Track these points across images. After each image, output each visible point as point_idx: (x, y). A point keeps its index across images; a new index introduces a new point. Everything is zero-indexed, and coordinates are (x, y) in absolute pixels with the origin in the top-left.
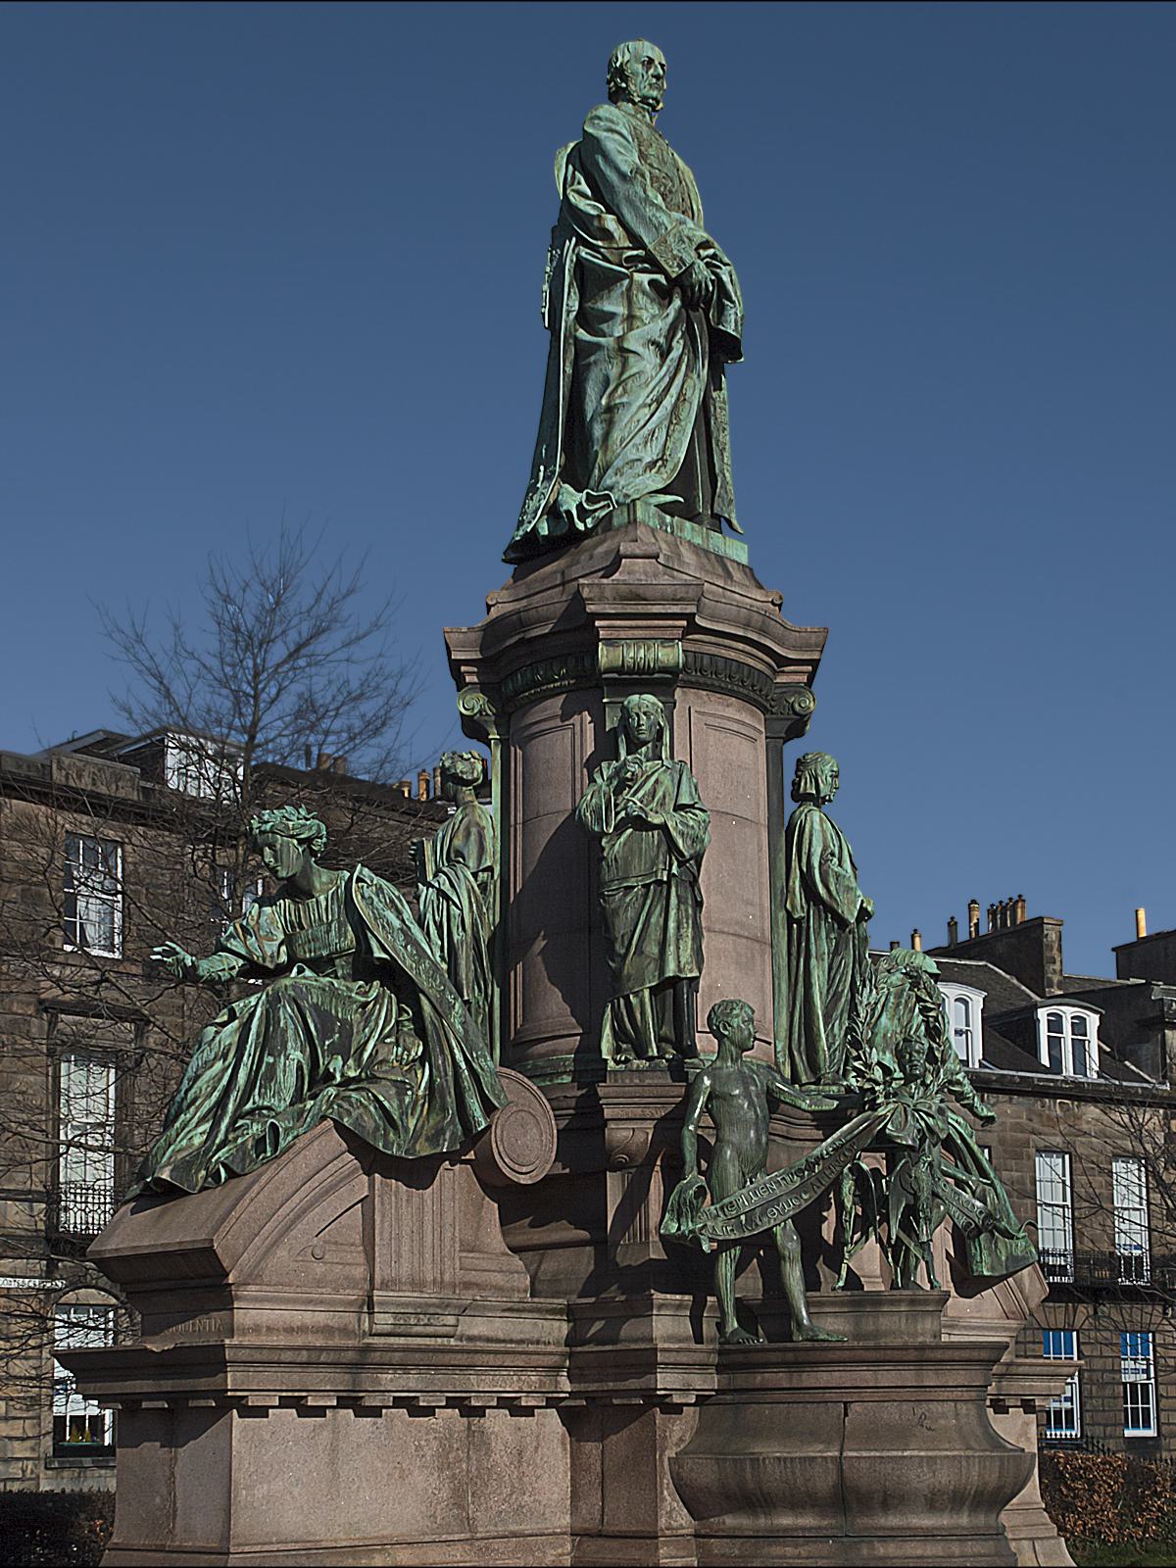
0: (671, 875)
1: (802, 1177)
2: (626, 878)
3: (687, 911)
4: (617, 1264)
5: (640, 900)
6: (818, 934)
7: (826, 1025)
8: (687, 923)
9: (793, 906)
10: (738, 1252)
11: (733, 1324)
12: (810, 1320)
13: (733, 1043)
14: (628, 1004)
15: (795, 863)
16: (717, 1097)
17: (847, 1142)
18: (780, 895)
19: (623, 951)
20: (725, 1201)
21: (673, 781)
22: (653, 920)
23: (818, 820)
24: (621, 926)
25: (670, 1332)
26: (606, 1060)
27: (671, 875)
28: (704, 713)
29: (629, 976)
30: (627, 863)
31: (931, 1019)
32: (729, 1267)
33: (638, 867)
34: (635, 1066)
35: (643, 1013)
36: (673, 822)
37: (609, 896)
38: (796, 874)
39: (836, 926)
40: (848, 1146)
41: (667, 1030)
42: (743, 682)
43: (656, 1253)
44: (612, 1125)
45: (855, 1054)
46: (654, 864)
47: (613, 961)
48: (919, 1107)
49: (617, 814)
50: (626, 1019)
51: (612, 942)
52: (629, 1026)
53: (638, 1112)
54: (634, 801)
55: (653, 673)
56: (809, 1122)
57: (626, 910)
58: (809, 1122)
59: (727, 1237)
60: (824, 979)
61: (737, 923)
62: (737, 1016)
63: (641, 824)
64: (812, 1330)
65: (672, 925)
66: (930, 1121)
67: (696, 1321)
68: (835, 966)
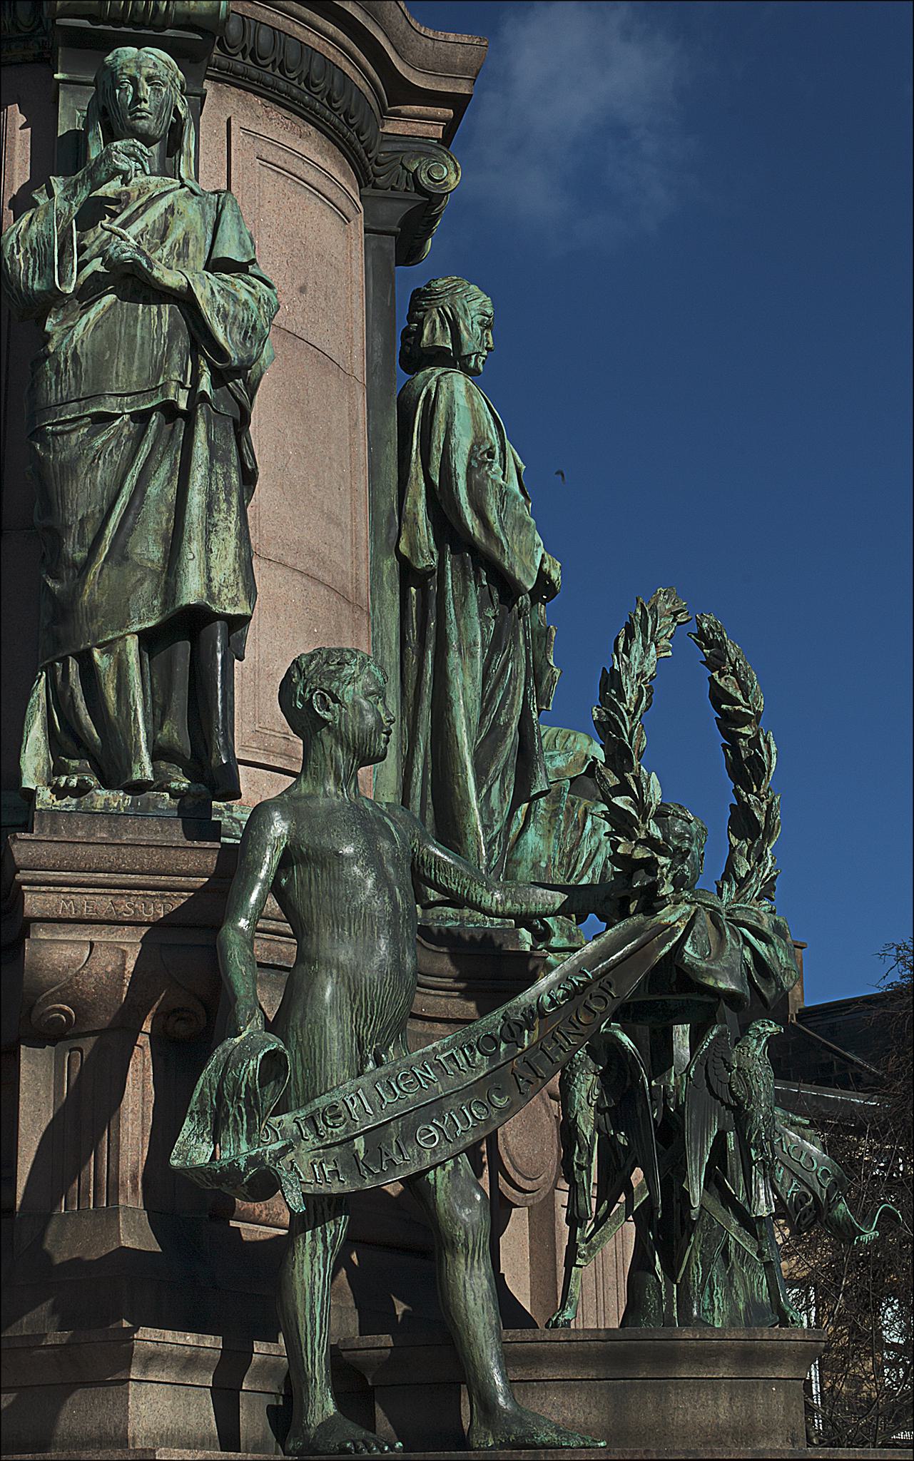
0: (197, 398)
1: (493, 1057)
2: (96, 397)
3: (227, 476)
4: (48, 1257)
5: (126, 448)
6: (462, 606)
7: (479, 787)
8: (227, 501)
9: (413, 546)
10: (342, 1230)
11: (323, 1405)
12: (510, 1395)
13: (340, 739)
14: (89, 673)
15: (416, 468)
16: (304, 859)
17: (598, 977)
18: (389, 524)
19: (80, 555)
20: (321, 1102)
21: (203, 215)
22: (153, 490)
23: (463, 388)
24: (82, 498)
25: (166, 1423)
26: (31, 794)
27: (197, 398)
28: (256, 135)
29: (94, 609)
30: (101, 365)
31: (743, 742)
32: (319, 1266)
33: (126, 373)
34: (99, 804)
35: (122, 687)
36: (205, 289)
37: (55, 434)
38: (418, 487)
39: (496, 595)
40: (595, 989)
41: (175, 732)
42: (329, 98)
43: (135, 1233)
44: (41, 933)
45: (613, 780)
46: (159, 370)
47: (57, 578)
48: (739, 916)
49: (82, 266)
50: (82, 705)
51: (55, 537)
52: (86, 719)
53: (102, 904)
54: (126, 237)
55: (164, 28)
56: (449, 982)
57: (93, 469)
58: (449, 982)
59: (324, 1189)
60: (474, 693)
61: (311, 553)
62: (353, 679)
63: (133, 282)
64: (521, 1422)
65: (196, 499)
66: (761, 947)
67: (226, 1398)
68: (495, 670)
